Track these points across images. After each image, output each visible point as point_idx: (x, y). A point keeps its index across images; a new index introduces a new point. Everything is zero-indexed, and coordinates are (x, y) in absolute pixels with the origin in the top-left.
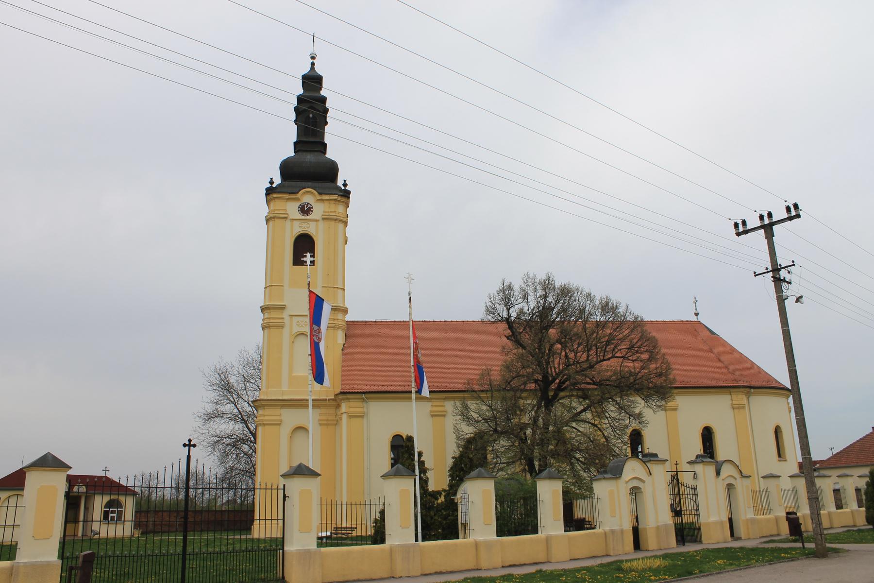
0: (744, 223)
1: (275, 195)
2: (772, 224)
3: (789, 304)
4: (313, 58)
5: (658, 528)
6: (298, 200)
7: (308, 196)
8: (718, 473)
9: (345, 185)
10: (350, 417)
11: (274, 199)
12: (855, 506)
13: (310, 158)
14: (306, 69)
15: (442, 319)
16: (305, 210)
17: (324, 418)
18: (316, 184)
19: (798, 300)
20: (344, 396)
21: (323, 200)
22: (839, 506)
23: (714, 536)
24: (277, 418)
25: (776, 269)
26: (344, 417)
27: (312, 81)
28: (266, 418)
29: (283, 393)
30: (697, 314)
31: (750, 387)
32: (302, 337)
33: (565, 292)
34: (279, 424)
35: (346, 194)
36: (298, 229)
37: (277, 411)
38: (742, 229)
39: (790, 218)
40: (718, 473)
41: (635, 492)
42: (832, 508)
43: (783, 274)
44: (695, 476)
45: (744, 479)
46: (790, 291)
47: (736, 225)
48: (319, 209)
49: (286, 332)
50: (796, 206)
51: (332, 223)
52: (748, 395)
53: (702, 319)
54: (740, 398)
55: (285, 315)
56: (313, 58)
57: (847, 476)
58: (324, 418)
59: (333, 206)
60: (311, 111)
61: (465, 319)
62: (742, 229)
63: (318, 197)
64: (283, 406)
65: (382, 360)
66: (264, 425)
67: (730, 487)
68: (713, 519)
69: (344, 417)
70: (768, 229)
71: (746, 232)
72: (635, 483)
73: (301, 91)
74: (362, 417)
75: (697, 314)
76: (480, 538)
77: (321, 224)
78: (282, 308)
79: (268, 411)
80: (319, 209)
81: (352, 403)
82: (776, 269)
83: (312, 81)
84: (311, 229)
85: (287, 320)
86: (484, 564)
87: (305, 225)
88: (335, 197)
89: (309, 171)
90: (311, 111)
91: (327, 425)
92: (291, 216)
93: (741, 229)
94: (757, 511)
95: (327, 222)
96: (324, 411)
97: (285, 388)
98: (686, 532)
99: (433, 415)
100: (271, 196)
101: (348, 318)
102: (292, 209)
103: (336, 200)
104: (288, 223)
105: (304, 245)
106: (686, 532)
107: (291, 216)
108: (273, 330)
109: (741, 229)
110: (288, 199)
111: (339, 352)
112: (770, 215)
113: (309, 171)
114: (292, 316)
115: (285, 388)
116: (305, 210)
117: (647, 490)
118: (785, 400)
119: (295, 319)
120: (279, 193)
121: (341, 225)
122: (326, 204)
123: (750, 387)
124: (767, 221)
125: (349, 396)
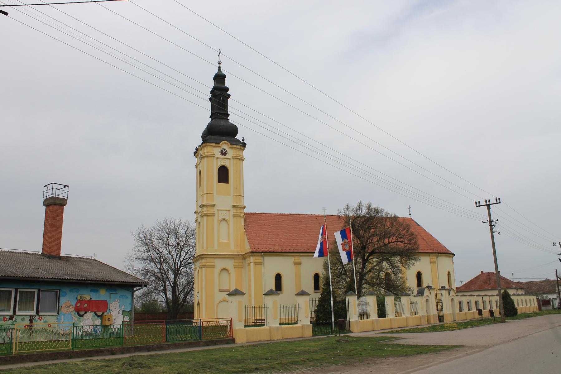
0: (479, 202)
1: (208, 144)
2: (490, 205)
3: (495, 235)
4: (219, 64)
5: (433, 315)
6: (220, 147)
7: (225, 145)
8: (449, 294)
9: (243, 140)
10: (256, 264)
11: (207, 146)
12: (475, 310)
13: (222, 122)
14: (216, 71)
15: (289, 213)
16: (224, 153)
17: (237, 264)
18: (228, 138)
19: (499, 233)
20: (253, 254)
21: (232, 148)
22: (461, 311)
23: (448, 320)
24: (213, 264)
25: (491, 222)
26: (252, 265)
27: (220, 78)
28: (207, 264)
29: (215, 251)
30: (410, 215)
31: (439, 253)
32: (224, 222)
33: (377, 211)
34: (214, 267)
35: (244, 145)
36: (220, 164)
37: (212, 260)
38: (478, 204)
39: (497, 203)
40: (449, 294)
41: (427, 300)
42: (458, 311)
43: (493, 223)
44: (442, 295)
45: (221, 299)
46: (495, 229)
47: (476, 203)
48: (231, 153)
49: (216, 219)
50: (499, 199)
51: (238, 161)
52: (437, 257)
53: (412, 217)
54: (434, 258)
55: (215, 209)
56: (219, 64)
57: (472, 295)
58: (237, 264)
59: (238, 151)
60: (220, 95)
61: (300, 213)
62: (478, 204)
63: (230, 146)
64: (215, 258)
65: (272, 234)
66: (206, 267)
67: (452, 299)
68: (448, 312)
69: (252, 265)
70: (488, 206)
71: (480, 206)
72: (427, 298)
73: (210, 120)
74: (261, 264)
75: (410, 215)
76: (391, 317)
77: (232, 160)
78: (213, 206)
79: (208, 260)
80: (231, 153)
81: (256, 258)
82: (491, 222)
83: (220, 78)
84: (227, 164)
85: (216, 212)
86: (393, 327)
87: (224, 161)
88: (239, 147)
89: (220, 130)
90: (220, 95)
91: (238, 268)
92: (217, 156)
93: (478, 205)
94: (412, 314)
95: (235, 160)
96: (236, 261)
97: (216, 248)
98: (441, 318)
99: (295, 264)
100: (206, 144)
101: (246, 211)
102: (216, 151)
103: (240, 148)
104: (215, 159)
105: (223, 175)
106: (441, 318)
107: (217, 156)
108: (209, 217)
109: (478, 205)
110: (214, 146)
111: (243, 230)
112: (489, 201)
113: (220, 130)
114: (218, 210)
115: (216, 248)
116: (224, 153)
117: (430, 299)
118: (451, 259)
119: (220, 212)
120: (210, 143)
121: (241, 162)
122: (235, 150)
123: (439, 253)
124: (488, 203)
125: (255, 254)
